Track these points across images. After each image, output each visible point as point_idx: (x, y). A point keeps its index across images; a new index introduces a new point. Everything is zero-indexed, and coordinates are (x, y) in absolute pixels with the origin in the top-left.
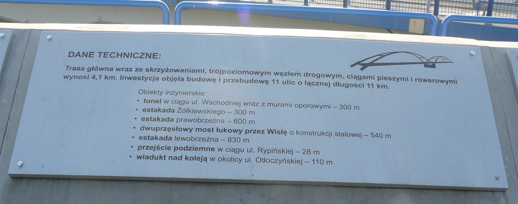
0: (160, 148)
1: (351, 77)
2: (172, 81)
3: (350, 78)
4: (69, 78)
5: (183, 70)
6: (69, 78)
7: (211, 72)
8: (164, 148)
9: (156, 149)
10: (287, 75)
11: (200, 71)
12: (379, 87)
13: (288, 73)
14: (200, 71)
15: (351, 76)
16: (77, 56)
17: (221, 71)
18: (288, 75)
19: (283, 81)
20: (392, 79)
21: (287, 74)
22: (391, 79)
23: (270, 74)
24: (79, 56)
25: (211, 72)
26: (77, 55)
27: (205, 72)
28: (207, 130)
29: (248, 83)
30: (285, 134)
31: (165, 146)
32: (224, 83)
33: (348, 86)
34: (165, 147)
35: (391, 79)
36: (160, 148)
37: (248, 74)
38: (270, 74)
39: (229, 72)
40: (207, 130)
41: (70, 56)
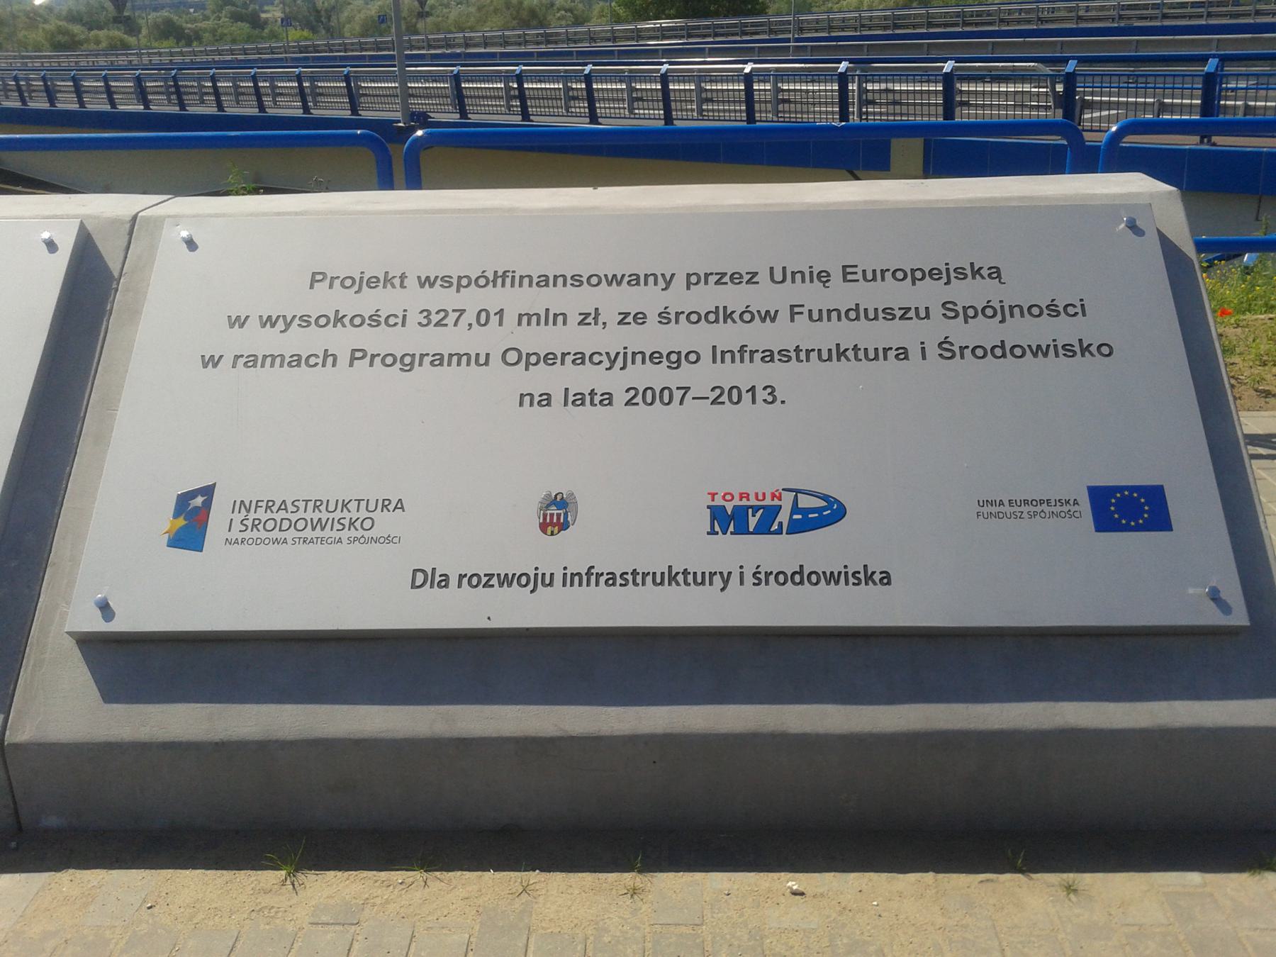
0: (382, 319)
1: (1080, 311)
2: (948, 283)
3: (1076, 314)
4: (281, 325)
5: (638, 276)
6: (281, 325)
7: (803, 356)
8: (397, 320)
9: (953, 279)
10: (590, 324)
11: (534, 319)
12: (843, 358)
13: (593, 316)
14: (534, 319)
15: (1079, 307)
16: (280, 511)
17: (1002, 307)
18: (593, 322)
19: (979, 501)
20: (898, 317)
21: (590, 320)
22: (894, 317)
23: (565, 323)
24: (401, 510)
25: (803, 356)
26: (235, 543)
27: (600, 322)
28: (367, 321)
29: (646, 275)
30: (824, 282)
31: (400, 315)
32: (688, 288)
33: (679, 361)
34: (401, 317)
35: (894, 317)
36: (382, 319)
37: (839, 319)
38: (565, 323)
39: (1035, 311)
40: (367, 321)
41: (283, 529)
